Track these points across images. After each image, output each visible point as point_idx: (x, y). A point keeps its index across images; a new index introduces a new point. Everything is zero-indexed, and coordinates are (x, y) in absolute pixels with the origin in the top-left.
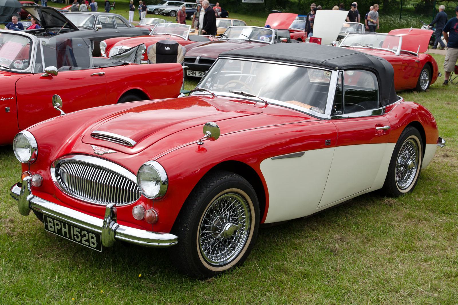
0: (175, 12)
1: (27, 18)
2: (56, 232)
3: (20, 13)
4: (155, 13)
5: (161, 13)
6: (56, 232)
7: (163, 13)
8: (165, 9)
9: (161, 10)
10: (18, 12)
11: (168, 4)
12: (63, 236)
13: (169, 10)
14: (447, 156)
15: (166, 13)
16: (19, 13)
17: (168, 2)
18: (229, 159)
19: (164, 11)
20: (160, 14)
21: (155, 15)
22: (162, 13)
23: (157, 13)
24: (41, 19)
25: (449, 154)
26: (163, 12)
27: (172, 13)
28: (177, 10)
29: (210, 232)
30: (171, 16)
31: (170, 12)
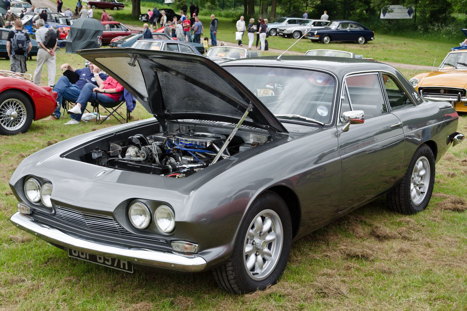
0: (300, 32)
1: (110, 43)
2: (88, 258)
3: (102, 37)
4: (271, 34)
5: (280, 34)
6: (88, 258)
7: (283, 33)
8: (287, 29)
9: (280, 30)
10: (98, 37)
11: (288, 22)
12: (126, 270)
13: (292, 30)
14: (395, 169)
15: (287, 34)
16: (100, 37)
17: (288, 19)
18: (277, 184)
19: (285, 32)
20: (279, 35)
21: (271, 37)
22: (282, 34)
23: (274, 34)
24: (149, 91)
25: (80, 64)
26: (284, 32)
27: (296, 34)
28: (305, 30)
29: (192, 152)
30: (294, 38)
31: (293, 32)
